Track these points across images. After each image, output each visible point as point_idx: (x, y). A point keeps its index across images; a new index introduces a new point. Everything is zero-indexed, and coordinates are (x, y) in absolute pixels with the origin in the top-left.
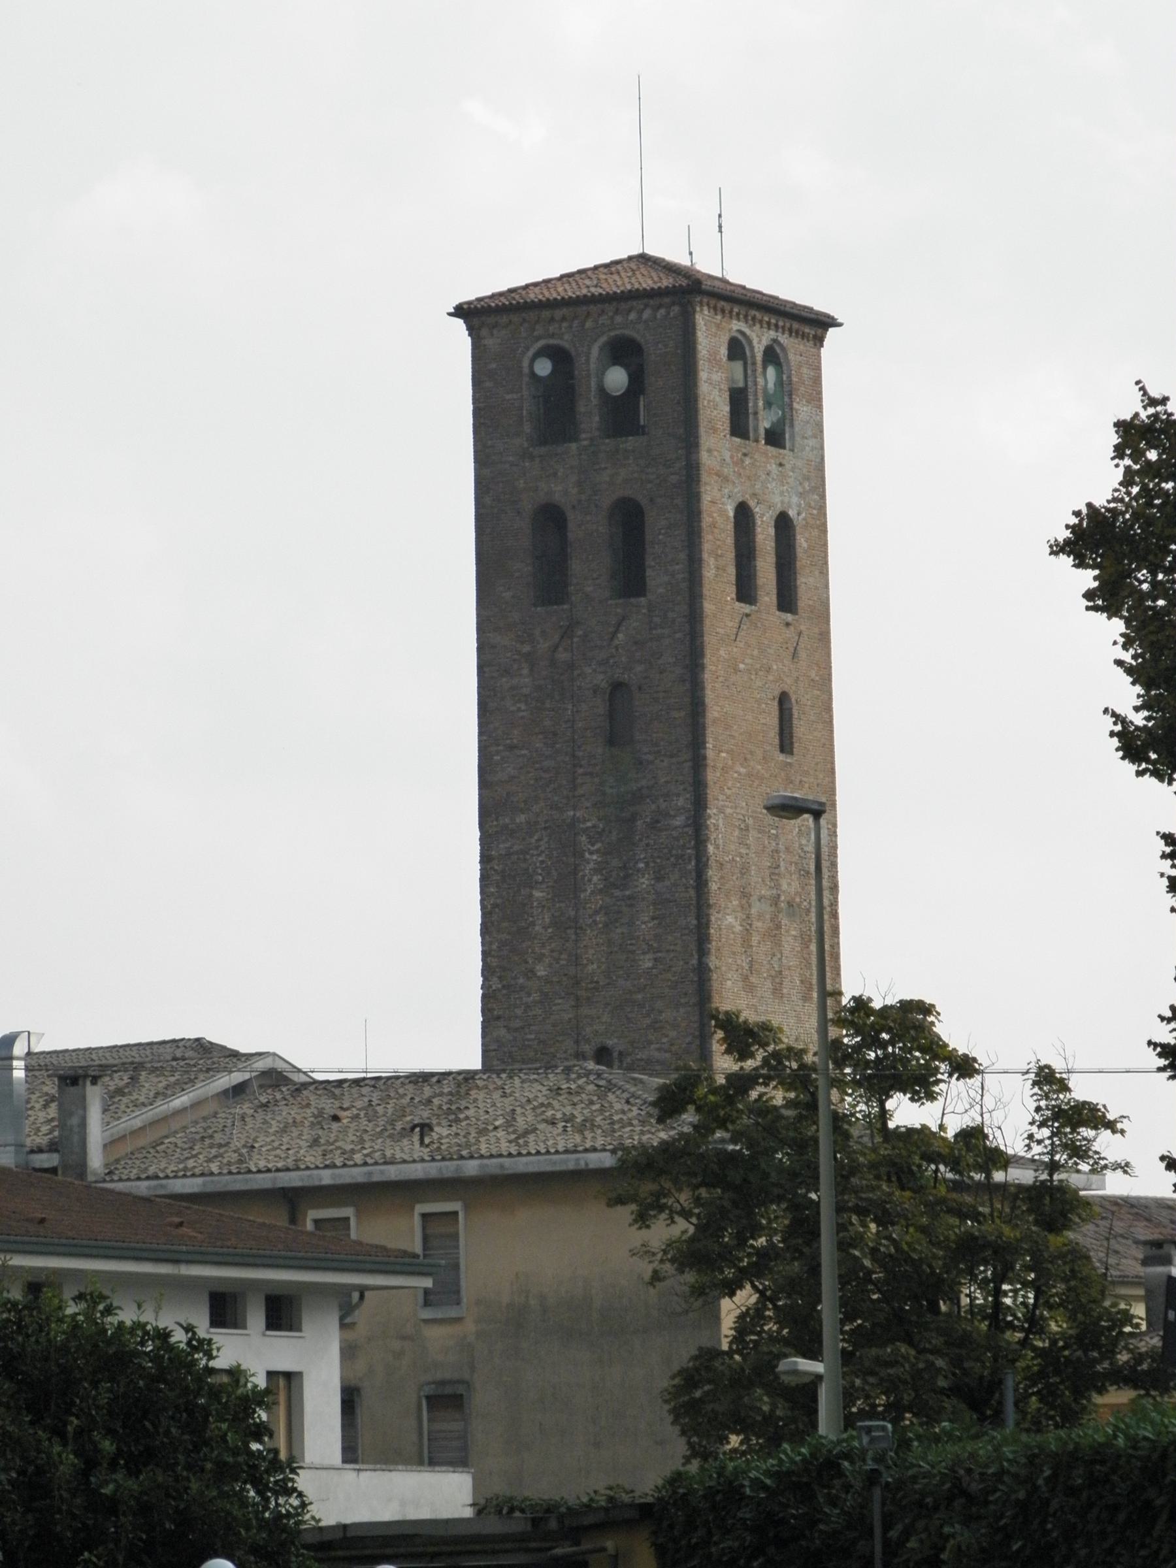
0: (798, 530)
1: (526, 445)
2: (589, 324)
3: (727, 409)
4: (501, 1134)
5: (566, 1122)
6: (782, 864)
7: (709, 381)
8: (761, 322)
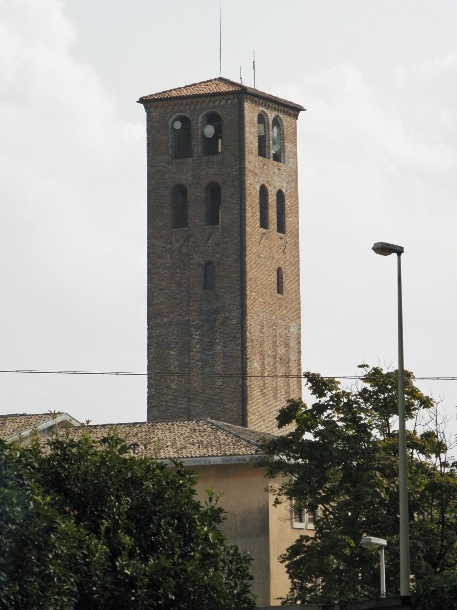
0: (286, 198)
1: (170, 159)
2: (198, 107)
3: (257, 144)
4: (170, 449)
5: (199, 444)
6: (278, 341)
7: (250, 132)
8: (271, 107)
